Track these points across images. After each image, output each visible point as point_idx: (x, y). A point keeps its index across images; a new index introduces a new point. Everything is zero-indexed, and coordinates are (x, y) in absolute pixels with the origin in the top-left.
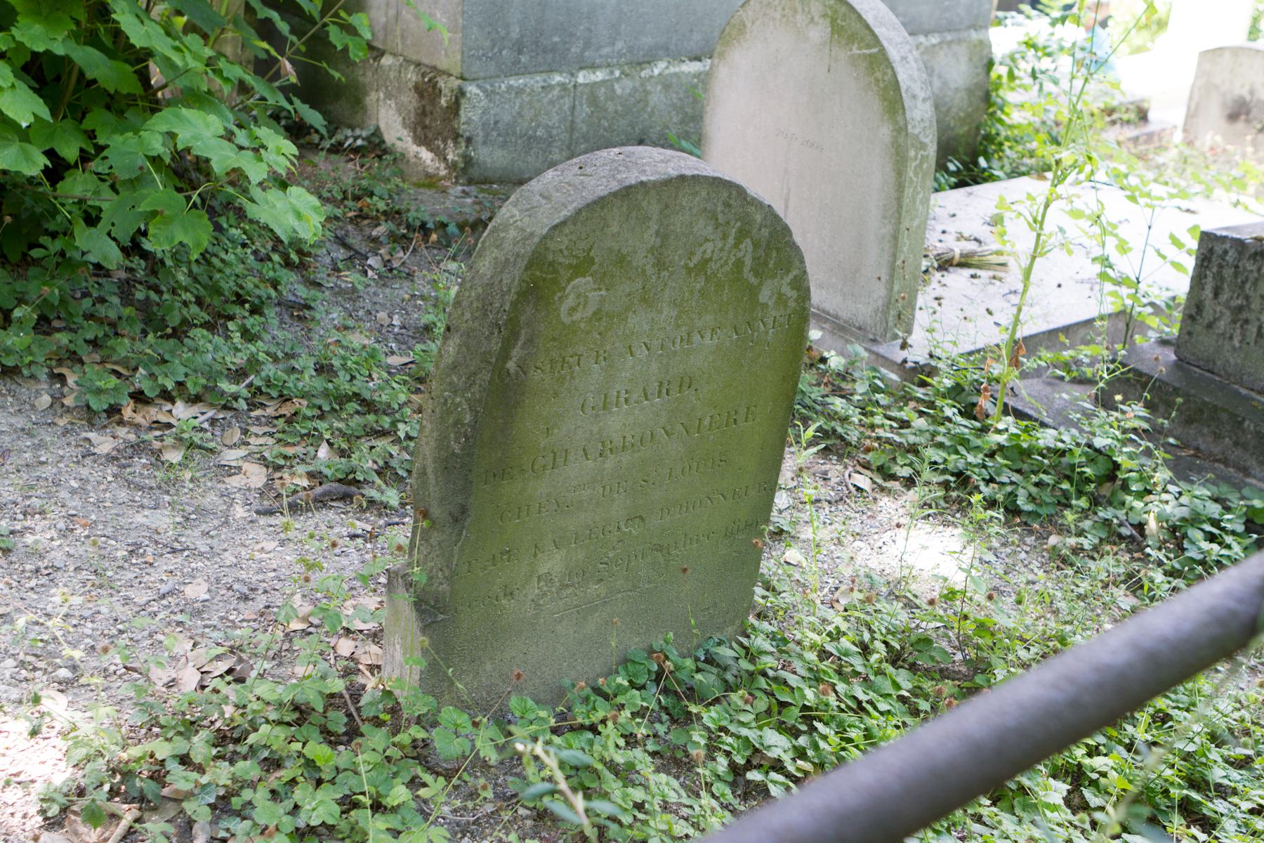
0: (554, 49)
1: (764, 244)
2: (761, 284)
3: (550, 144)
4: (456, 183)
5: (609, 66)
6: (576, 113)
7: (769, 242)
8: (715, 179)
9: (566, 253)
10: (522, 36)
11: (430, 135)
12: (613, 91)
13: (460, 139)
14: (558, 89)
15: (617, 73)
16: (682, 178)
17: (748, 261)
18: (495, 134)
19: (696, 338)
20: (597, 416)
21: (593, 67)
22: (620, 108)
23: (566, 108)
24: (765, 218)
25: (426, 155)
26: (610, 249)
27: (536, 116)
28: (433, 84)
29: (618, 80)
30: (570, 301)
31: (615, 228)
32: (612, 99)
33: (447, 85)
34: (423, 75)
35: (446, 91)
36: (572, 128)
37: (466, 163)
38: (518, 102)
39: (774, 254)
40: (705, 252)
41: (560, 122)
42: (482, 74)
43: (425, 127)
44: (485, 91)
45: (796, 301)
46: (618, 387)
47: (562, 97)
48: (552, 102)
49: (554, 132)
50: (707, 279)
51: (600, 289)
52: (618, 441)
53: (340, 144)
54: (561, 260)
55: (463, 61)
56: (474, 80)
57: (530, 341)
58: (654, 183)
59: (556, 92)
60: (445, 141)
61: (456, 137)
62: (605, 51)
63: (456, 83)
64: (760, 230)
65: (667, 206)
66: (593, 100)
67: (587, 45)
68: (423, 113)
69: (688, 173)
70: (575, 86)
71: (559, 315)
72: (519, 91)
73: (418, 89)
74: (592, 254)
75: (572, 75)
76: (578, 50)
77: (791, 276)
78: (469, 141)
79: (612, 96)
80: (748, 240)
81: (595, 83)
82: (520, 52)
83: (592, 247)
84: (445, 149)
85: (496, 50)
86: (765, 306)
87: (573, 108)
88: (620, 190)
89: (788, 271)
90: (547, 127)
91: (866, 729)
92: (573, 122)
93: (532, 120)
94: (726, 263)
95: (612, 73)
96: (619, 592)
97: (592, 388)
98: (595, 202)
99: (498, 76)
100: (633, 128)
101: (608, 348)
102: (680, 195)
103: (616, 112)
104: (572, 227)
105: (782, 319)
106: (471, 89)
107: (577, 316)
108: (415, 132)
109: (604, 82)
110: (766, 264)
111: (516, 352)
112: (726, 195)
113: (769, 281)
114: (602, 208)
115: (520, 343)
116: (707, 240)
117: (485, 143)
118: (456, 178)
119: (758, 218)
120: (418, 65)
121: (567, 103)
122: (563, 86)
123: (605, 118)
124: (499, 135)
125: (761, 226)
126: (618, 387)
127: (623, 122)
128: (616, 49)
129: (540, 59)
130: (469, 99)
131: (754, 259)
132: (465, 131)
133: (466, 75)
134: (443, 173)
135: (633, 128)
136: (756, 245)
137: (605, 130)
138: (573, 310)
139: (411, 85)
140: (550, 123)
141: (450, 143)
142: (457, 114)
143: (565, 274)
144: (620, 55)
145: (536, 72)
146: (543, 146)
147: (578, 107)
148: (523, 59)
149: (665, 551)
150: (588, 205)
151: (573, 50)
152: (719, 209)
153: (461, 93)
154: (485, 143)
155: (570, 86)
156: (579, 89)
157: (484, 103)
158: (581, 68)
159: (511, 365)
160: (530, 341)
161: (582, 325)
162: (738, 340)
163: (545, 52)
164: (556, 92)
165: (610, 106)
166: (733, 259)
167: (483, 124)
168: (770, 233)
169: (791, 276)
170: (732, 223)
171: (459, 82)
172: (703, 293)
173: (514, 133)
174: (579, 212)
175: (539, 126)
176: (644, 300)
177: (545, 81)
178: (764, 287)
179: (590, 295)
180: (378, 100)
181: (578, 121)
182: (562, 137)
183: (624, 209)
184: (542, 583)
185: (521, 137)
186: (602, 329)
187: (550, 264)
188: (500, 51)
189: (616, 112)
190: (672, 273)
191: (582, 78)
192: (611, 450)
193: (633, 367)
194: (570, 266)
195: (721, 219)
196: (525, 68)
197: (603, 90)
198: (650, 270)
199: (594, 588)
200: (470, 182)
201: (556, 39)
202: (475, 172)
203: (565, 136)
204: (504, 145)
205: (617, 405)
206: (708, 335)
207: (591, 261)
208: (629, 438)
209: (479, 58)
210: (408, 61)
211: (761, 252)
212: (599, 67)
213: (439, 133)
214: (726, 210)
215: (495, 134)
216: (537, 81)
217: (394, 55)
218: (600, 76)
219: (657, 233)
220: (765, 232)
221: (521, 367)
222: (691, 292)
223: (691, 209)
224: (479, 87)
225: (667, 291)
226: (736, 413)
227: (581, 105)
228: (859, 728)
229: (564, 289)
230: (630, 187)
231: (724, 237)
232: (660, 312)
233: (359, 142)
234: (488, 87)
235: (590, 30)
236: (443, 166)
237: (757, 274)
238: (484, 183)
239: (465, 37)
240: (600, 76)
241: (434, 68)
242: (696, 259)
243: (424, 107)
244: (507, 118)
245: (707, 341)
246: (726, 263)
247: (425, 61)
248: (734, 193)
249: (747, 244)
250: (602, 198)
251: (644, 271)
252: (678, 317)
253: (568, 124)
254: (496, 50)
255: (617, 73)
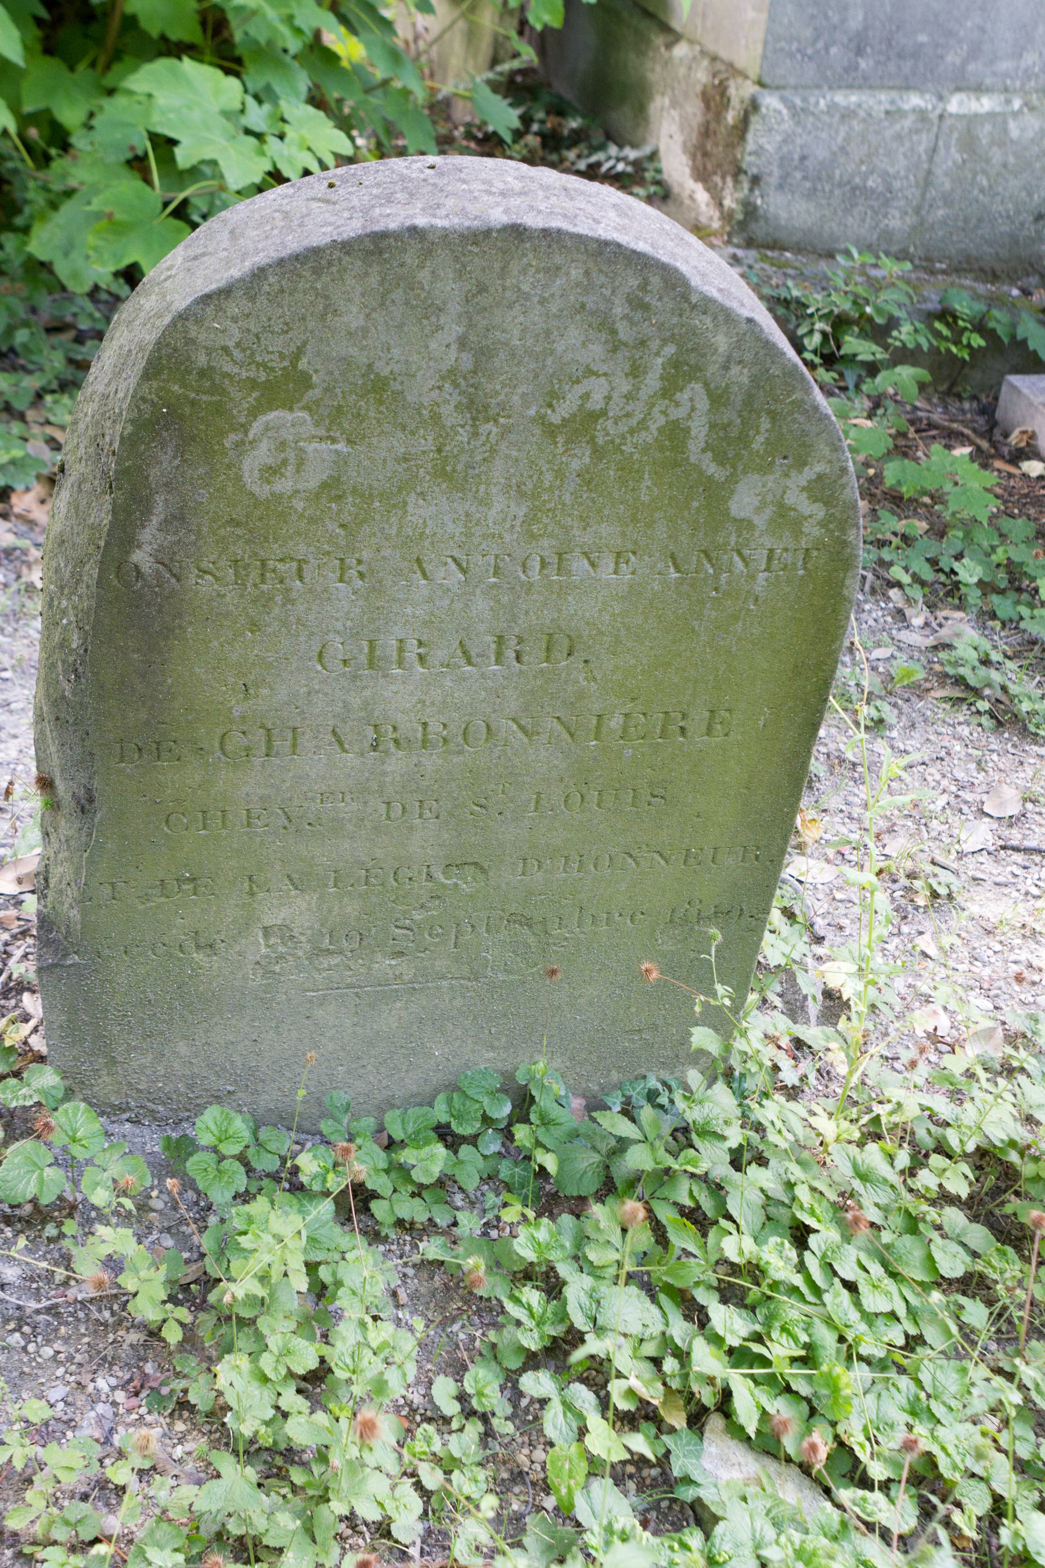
0: (916, 53)
1: (738, 400)
2: (732, 480)
3: (886, 203)
4: (729, 242)
5: (1006, 90)
6: (936, 159)
7: (749, 401)
8: (604, 244)
9: (237, 354)
10: (866, 28)
11: (709, 166)
12: (1005, 131)
13: (742, 177)
14: (912, 118)
15: (1017, 104)
16: (517, 232)
17: (699, 429)
18: (798, 175)
19: (579, 565)
20: (355, 677)
21: (979, 89)
22: (1012, 160)
23: (921, 149)
24: (738, 345)
25: (702, 196)
26: (346, 361)
27: (869, 155)
28: (722, 89)
29: (1015, 115)
30: (262, 454)
31: (353, 317)
32: (1001, 144)
33: (740, 91)
34: (714, 76)
35: (735, 102)
36: (927, 181)
37: (747, 214)
38: (843, 130)
39: (765, 424)
40: (586, 397)
41: (908, 170)
42: (792, 81)
43: (706, 154)
44: (791, 107)
45: (822, 524)
46: (398, 632)
47: (918, 131)
48: (898, 137)
49: (897, 184)
50: (598, 453)
51: (334, 440)
52: (410, 727)
53: (598, 164)
54: (229, 368)
55: (764, 57)
56: (778, 88)
57: (177, 519)
58: (446, 235)
59: (908, 123)
60: (723, 178)
61: (738, 172)
62: (1005, 65)
63: (749, 89)
64: (726, 368)
65: (482, 289)
66: (969, 143)
67: (975, 52)
68: (706, 132)
69: (534, 221)
70: (941, 117)
71: (239, 478)
72: (848, 115)
73: (706, 98)
74: (303, 364)
75: (941, 98)
76: (958, 61)
77: (808, 474)
78: (756, 180)
79: (1001, 139)
80: (698, 387)
81: (976, 115)
82: (859, 52)
83: (300, 352)
84: (722, 189)
85: (820, 44)
86: (745, 525)
87: (934, 150)
88: (359, 239)
89: (801, 463)
90: (885, 175)
91: (808, 1346)
92: (929, 172)
93: (862, 162)
94: (642, 425)
95: (1008, 102)
96: (444, 978)
97: (339, 626)
98: (296, 257)
99: (818, 87)
100: (1030, 195)
101: (366, 555)
102: (515, 267)
103: (1005, 165)
104: (247, 306)
105: (788, 557)
106: (770, 102)
107: (284, 485)
108: (694, 160)
109: (991, 115)
110: (744, 440)
111: (149, 535)
112: (634, 282)
113: (754, 478)
114: (317, 272)
115: (155, 520)
116: (590, 372)
117: (780, 187)
118: (730, 234)
119: (722, 342)
120: (714, 59)
121: (924, 142)
122: (922, 115)
123: (984, 172)
124: (805, 178)
125: (729, 359)
126: (398, 632)
127: (1014, 183)
128: (1023, 64)
129: (892, 67)
130: (763, 118)
131: (713, 426)
132: (750, 164)
133: (767, 80)
134: (716, 225)
135: (1030, 195)
136: (718, 398)
137: (982, 191)
138: (271, 472)
139: (699, 89)
140: (891, 171)
141: (729, 181)
142: (742, 137)
143: (243, 401)
144: (1028, 75)
145: (882, 87)
146: (876, 204)
147: (942, 151)
148: (863, 64)
149: (537, 929)
150: (281, 262)
151: (949, 58)
152: (618, 311)
153: (753, 106)
154: (780, 187)
155: (934, 116)
156: (948, 122)
157: (788, 125)
158: (958, 89)
159: (142, 557)
160: (177, 519)
161: (299, 505)
162: (680, 582)
163: (900, 56)
164: (908, 123)
165: (997, 155)
166: (662, 421)
167: (782, 159)
168: (754, 379)
169: (808, 474)
170: (654, 345)
171: (756, 89)
172: (587, 479)
173: (830, 178)
174: (259, 274)
175: (872, 172)
176: (442, 473)
177: (892, 102)
178: (741, 487)
179: (311, 447)
180: (662, 109)
181: (938, 171)
182: (908, 193)
183: (374, 280)
184: (272, 941)
185: (840, 185)
186: (346, 518)
187: (202, 373)
188: (827, 49)
189: (1005, 165)
190: (506, 430)
191: (956, 104)
192: (396, 741)
193: (430, 600)
194: (253, 384)
195: (624, 332)
196: (865, 78)
197: (988, 128)
198: (450, 415)
199: (385, 964)
200: (750, 243)
201: (923, 38)
202: (758, 230)
203: (913, 193)
204: (810, 195)
205: (400, 664)
206: (608, 562)
207: (305, 381)
208: (435, 727)
209: (791, 55)
210: (703, 53)
211: (728, 415)
212: (990, 91)
213: (719, 166)
214: (638, 316)
215: (798, 175)
216: (878, 101)
217: (691, 42)
218: (986, 104)
219: (463, 343)
220: (740, 376)
221: (165, 560)
222: (560, 474)
223: (543, 301)
224: (783, 99)
225: (499, 463)
226: (684, 716)
227: (947, 148)
228: (796, 1340)
229: (245, 428)
230: (384, 235)
231: (636, 372)
232: (485, 502)
233: (620, 167)
234: (798, 102)
235: (982, 30)
236: (717, 214)
237: (721, 459)
238: (772, 248)
239: (772, 19)
240: (986, 104)
241: (731, 66)
242: (564, 410)
243: (708, 122)
244: (821, 153)
245: (606, 572)
246: (642, 425)
247: (724, 54)
248: (655, 281)
249: (692, 393)
250: (316, 252)
251: (436, 418)
252: (530, 519)
253: (921, 174)
254: (820, 44)
255: (1017, 104)
